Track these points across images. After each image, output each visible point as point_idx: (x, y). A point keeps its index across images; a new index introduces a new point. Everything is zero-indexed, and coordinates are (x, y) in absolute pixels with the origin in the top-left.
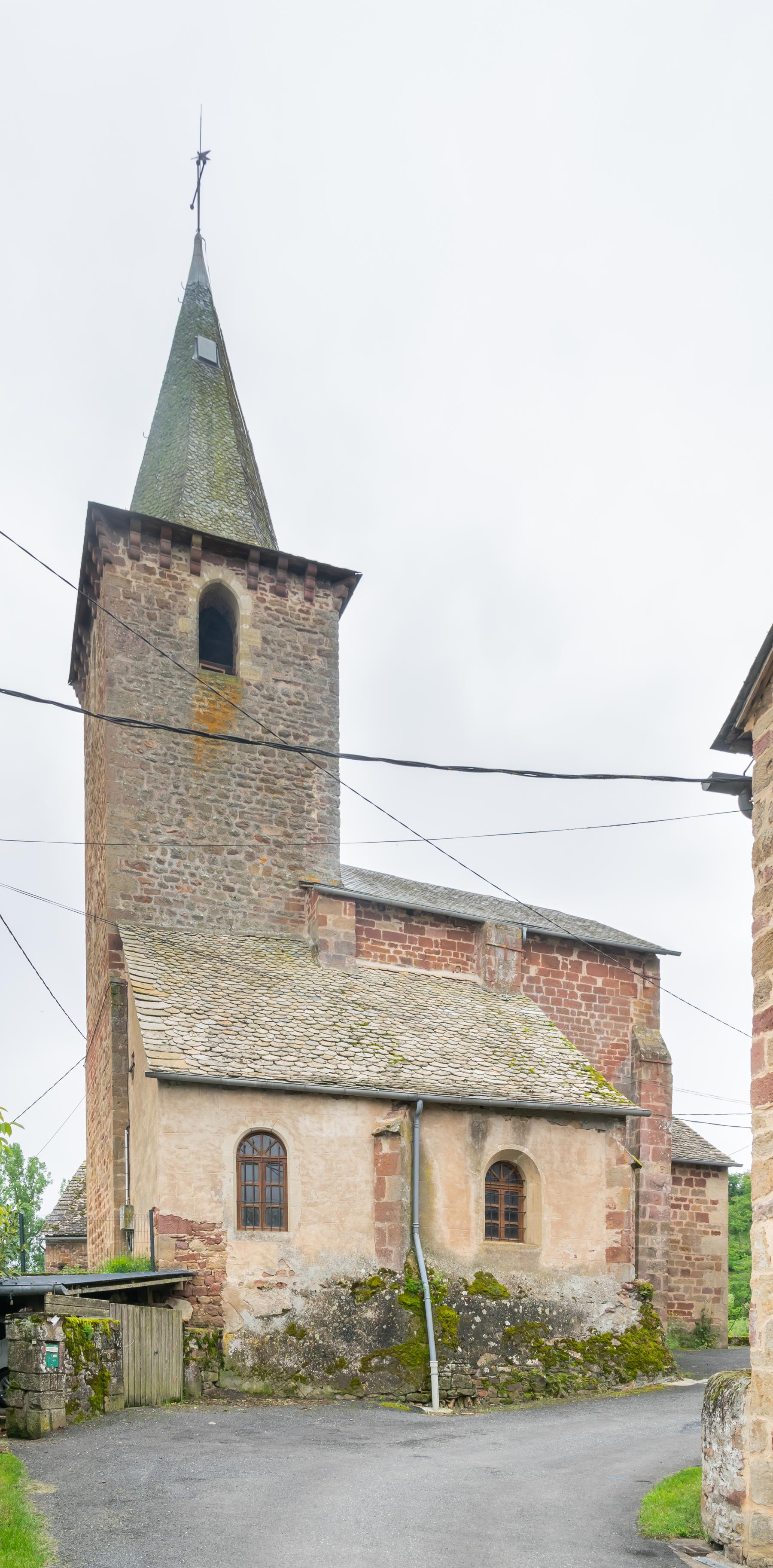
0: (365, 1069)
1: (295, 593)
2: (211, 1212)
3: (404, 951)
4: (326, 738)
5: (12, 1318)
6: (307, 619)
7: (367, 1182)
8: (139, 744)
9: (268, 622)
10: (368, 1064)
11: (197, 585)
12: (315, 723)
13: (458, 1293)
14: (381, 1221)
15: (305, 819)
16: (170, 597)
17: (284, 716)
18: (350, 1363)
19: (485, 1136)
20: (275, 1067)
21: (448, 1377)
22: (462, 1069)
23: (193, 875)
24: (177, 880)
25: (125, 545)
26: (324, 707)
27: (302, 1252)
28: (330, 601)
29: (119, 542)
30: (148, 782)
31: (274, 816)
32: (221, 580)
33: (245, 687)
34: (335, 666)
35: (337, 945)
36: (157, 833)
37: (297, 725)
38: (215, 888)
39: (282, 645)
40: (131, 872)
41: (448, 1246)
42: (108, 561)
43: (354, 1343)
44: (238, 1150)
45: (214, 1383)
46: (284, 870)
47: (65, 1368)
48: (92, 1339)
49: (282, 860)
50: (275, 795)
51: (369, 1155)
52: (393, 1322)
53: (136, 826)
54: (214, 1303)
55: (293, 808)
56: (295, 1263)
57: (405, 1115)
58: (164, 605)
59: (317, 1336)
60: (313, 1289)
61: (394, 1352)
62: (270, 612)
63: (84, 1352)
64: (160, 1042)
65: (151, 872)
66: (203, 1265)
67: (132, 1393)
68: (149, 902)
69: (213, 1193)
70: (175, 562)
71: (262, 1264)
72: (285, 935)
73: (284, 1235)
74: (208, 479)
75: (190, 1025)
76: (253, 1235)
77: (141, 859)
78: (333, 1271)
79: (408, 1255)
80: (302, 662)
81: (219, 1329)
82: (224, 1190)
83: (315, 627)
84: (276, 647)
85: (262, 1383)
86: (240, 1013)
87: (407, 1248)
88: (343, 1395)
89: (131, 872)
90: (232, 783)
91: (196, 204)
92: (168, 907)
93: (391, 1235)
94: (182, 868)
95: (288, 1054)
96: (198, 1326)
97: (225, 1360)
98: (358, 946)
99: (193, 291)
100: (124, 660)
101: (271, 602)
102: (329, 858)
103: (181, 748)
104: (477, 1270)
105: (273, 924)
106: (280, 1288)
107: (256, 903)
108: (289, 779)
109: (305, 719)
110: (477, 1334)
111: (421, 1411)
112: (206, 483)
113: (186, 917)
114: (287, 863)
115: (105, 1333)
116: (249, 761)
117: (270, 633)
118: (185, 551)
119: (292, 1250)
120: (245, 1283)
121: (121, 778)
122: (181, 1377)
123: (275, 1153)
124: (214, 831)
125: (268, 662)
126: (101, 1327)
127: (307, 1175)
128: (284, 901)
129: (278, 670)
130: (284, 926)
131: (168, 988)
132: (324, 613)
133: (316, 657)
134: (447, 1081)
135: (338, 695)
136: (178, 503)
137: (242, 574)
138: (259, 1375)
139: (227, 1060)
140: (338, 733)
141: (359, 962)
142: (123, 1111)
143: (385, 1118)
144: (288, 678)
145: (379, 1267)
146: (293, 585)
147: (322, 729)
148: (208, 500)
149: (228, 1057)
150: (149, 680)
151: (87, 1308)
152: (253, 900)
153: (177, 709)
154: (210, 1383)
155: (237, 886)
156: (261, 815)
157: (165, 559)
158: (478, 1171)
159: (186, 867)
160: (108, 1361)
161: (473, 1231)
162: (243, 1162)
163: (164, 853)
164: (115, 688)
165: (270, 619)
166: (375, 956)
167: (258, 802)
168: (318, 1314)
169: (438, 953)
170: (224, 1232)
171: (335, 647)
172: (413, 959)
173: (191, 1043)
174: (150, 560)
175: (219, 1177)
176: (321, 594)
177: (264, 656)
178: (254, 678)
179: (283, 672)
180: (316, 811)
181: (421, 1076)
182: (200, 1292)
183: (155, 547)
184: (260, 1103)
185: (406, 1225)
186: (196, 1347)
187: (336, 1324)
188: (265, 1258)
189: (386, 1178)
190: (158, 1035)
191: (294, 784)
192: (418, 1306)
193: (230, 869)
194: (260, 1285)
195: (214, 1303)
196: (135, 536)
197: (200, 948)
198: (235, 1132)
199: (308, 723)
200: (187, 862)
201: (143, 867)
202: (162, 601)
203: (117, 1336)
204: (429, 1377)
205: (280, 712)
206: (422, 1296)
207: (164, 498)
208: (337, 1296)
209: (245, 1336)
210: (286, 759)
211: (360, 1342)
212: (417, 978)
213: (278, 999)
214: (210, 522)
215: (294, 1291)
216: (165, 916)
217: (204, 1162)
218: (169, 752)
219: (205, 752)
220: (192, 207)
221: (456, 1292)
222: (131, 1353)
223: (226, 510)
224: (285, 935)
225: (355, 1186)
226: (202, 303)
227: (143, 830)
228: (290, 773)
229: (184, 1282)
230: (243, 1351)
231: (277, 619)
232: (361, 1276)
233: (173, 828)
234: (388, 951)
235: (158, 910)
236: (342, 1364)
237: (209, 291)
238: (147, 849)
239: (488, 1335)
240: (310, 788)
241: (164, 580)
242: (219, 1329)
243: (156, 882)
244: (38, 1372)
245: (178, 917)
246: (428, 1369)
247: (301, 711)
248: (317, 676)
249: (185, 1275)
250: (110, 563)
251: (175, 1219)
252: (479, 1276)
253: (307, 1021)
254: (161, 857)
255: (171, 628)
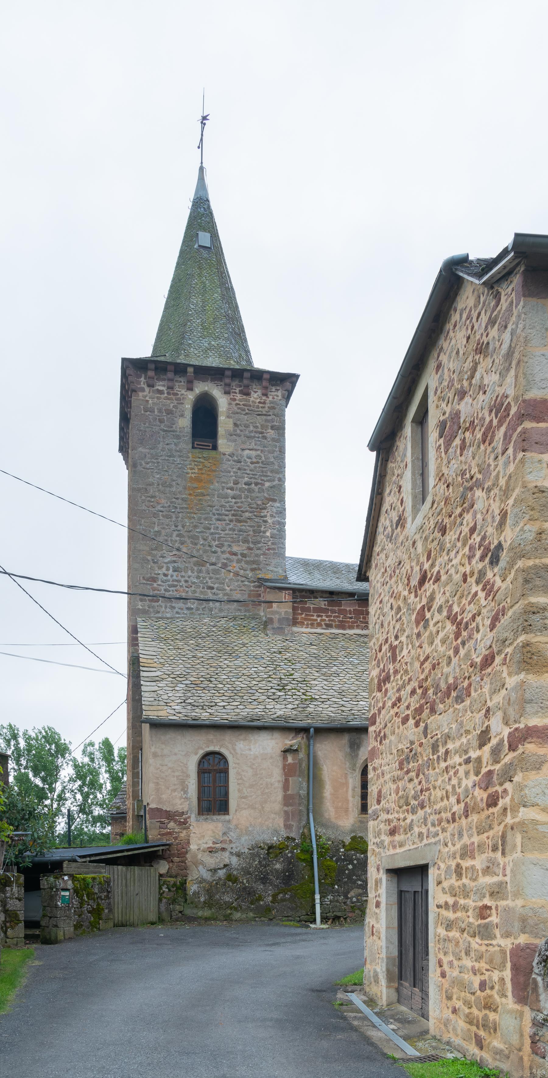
0: (283, 706)
1: (256, 392)
2: (181, 805)
3: (327, 619)
4: (276, 482)
5: (44, 876)
6: (264, 407)
7: (279, 781)
8: (153, 502)
9: (237, 413)
10: (287, 703)
11: (191, 397)
12: (269, 474)
13: (338, 850)
14: (287, 806)
15: (262, 537)
16: (173, 407)
17: (248, 472)
18: (265, 897)
19: (359, 747)
20: (224, 711)
21: (327, 905)
22: (351, 702)
23: (186, 581)
24: (176, 586)
25: (145, 379)
26: (275, 462)
27: (238, 828)
28: (279, 393)
29: (141, 377)
30: (158, 525)
31: (241, 537)
32: (206, 391)
33: (222, 456)
34: (283, 434)
35: (279, 620)
36: (163, 557)
37: (257, 477)
38: (201, 589)
39: (247, 426)
40: (147, 584)
41: (333, 820)
42: (134, 391)
43: (268, 884)
44: (199, 765)
45: (181, 912)
46: (248, 572)
47: (73, 904)
48: (92, 887)
49: (246, 566)
50: (242, 524)
51: (280, 764)
52: (293, 871)
53: (150, 554)
54: (182, 862)
55: (254, 531)
56: (232, 835)
57: (303, 738)
58: (169, 412)
59: (245, 881)
60: (243, 851)
61: (293, 889)
62: (239, 406)
63: (87, 895)
64: (152, 699)
65: (159, 583)
66: (176, 838)
67: (120, 919)
68: (158, 602)
69: (182, 793)
70: (177, 384)
71: (212, 836)
72: (247, 614)
73: (227, 817)
74: (201, 325)
75: (173, 685)
76: (207, 819)
77: (153, 575)
78: (256, 839)
79: (304, 827)
80: (260, 435)
81: (185, 878)
82: (189, 790)
83: (269, 411)
84: (243, 428)
85: (210, 912)
86: (208, 674)
87: (304, 822)
88: (260, 918)
89: (147, 584)
90: (213, 519)
91: (200, 146)
92: (170, 604)
93: (293, 815)
94: (180, 578)
95: (235, 700)
96: (171, 877)
97: (188, 897)
98: (294, 618)
99: (197, 202)
100: (143, 450)
101: (240, 400)
102: (278, 561)
103: (180, 501)
104: (353, 835)
105: (240, 608)
106: (223, 851)
107: (228, 595)
108: (251, 512)
109: (262, 472)
110: (349, 877)
111: (308, 926)
112: (200, 327)
113: (182, 609)
114: (249, 567)
115: (100, 883)
116: (224, 504)
117: (239, 420)
118: (184, 377)
119: (231, 827)
120: (202, 849)
121: (141, 525)
122: (157, 908)
123: (222, 766)
124: (201, 552)
125: (237, 438)
126: (98, 880)
127: (241, 779)
128: (247, 592)
129: (244, 443)
130: (247, 609)
131: (163, 661)
132: (275, 402)
133: (270, 431)
134: (337, 711)
135: (285, 453)
136: (182, 344)
137: (221, 385)
138: (208, 906)
139: (193, 708)
140: (285, 478)
141: (295, 629)
142: (138, 738)
143: (290, 741)
144: (251, 447)
145: (285, 836)
146: (254, 386)
147: (274, 477)
148: (201, 339)
149: (194, 706)
150: (159, 460)
151: (91, 869)
152: (227, 593)
153: (177, 477)
154: (177, 912)
155: (216, 586)
156: (232, 538)
157: (170, 384)
158: (355, 770)
159: (182, 576)
160: (102, 899)
161: (350, 809)
162: (201, 772)
163: (168, 569)
164: (137, 469)
165: (239, 411)
166: (308, 625)
167: (230, 530)
168: (245, 867)
169: (351, 618)
170: (189, 817)
171: (283, 422)
172: (334, 624)
173: (172, 698)
174: (161, 386)
175: (186, 783)
176: (274, 390)
177: (235, 435)
178: (228, 450)
179: (248, 444)
180: (270, 531)
181: (321, 709)
182: (174, 855)
183: (164, 377)
184: (212, 735)
185: (303, 808)
186: (167, 890)
187: (257, 873)
188: (214, 832)
189: (290, 778)
190: (153, 695)
191: (254, 515)
192: (309, 860)
193: (211, 575)
194: (210, 850)
195: (182, 862)
196: (151, 373)
197: (189, 630)
198: (196, 754)
199: (264, 474)
200: (183, 574)
201: (154, 580)
202: (168, 410)
203: (109, 885)
204: (314, 905)
205: (245, 470)
206: (312, 853)
207: (174, 340)
208: (258, 855)
209: (200, 882)
210: (249, 500)
211: (271, 884)
212: (335, 637)
213: (236, 662)
214: (202, 353)
215: (231, 853)
216: (168, 610)
217: (177, 774)
218: (172, 505)
219: (195, 501)
220: (199, 147)
221: (336, 850)
222: (119, 894)
223: (213, 343)
224: (247, 614)
225: (272, 785)
226: (202, 209)
227: (154, 556)
228: (252, 508)
229: (163, 850)
230: (199, 892)
231: (244, 410)
232: (274, 842)
233: (174, 553)
234: (316, 620)
235: (163, 606)
236: (260, 899)
237: (208, 200)
238: (157, 568)
239: (357, 876)
240: (266, 516)
241: (170, 396)
242: (185, 878)
243: (162, 588)
244: (56, 906)
245: (177, 610)
246: (314, 900)
247: (260, 467)
248: (270, 443)
249: (163, 845)
250: (135, 391)
251: (159, 810)
252: (353, 838)
253: (251, 676)
254: (166, 572)
255: (174, 426)
